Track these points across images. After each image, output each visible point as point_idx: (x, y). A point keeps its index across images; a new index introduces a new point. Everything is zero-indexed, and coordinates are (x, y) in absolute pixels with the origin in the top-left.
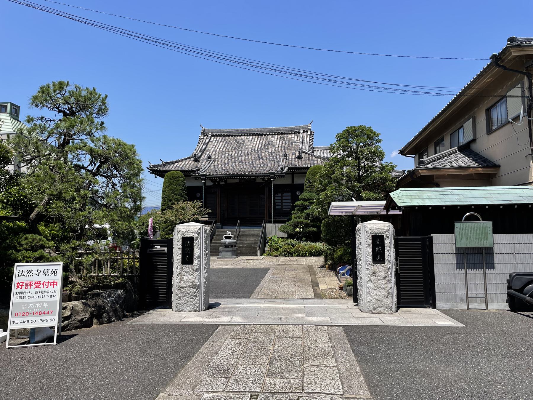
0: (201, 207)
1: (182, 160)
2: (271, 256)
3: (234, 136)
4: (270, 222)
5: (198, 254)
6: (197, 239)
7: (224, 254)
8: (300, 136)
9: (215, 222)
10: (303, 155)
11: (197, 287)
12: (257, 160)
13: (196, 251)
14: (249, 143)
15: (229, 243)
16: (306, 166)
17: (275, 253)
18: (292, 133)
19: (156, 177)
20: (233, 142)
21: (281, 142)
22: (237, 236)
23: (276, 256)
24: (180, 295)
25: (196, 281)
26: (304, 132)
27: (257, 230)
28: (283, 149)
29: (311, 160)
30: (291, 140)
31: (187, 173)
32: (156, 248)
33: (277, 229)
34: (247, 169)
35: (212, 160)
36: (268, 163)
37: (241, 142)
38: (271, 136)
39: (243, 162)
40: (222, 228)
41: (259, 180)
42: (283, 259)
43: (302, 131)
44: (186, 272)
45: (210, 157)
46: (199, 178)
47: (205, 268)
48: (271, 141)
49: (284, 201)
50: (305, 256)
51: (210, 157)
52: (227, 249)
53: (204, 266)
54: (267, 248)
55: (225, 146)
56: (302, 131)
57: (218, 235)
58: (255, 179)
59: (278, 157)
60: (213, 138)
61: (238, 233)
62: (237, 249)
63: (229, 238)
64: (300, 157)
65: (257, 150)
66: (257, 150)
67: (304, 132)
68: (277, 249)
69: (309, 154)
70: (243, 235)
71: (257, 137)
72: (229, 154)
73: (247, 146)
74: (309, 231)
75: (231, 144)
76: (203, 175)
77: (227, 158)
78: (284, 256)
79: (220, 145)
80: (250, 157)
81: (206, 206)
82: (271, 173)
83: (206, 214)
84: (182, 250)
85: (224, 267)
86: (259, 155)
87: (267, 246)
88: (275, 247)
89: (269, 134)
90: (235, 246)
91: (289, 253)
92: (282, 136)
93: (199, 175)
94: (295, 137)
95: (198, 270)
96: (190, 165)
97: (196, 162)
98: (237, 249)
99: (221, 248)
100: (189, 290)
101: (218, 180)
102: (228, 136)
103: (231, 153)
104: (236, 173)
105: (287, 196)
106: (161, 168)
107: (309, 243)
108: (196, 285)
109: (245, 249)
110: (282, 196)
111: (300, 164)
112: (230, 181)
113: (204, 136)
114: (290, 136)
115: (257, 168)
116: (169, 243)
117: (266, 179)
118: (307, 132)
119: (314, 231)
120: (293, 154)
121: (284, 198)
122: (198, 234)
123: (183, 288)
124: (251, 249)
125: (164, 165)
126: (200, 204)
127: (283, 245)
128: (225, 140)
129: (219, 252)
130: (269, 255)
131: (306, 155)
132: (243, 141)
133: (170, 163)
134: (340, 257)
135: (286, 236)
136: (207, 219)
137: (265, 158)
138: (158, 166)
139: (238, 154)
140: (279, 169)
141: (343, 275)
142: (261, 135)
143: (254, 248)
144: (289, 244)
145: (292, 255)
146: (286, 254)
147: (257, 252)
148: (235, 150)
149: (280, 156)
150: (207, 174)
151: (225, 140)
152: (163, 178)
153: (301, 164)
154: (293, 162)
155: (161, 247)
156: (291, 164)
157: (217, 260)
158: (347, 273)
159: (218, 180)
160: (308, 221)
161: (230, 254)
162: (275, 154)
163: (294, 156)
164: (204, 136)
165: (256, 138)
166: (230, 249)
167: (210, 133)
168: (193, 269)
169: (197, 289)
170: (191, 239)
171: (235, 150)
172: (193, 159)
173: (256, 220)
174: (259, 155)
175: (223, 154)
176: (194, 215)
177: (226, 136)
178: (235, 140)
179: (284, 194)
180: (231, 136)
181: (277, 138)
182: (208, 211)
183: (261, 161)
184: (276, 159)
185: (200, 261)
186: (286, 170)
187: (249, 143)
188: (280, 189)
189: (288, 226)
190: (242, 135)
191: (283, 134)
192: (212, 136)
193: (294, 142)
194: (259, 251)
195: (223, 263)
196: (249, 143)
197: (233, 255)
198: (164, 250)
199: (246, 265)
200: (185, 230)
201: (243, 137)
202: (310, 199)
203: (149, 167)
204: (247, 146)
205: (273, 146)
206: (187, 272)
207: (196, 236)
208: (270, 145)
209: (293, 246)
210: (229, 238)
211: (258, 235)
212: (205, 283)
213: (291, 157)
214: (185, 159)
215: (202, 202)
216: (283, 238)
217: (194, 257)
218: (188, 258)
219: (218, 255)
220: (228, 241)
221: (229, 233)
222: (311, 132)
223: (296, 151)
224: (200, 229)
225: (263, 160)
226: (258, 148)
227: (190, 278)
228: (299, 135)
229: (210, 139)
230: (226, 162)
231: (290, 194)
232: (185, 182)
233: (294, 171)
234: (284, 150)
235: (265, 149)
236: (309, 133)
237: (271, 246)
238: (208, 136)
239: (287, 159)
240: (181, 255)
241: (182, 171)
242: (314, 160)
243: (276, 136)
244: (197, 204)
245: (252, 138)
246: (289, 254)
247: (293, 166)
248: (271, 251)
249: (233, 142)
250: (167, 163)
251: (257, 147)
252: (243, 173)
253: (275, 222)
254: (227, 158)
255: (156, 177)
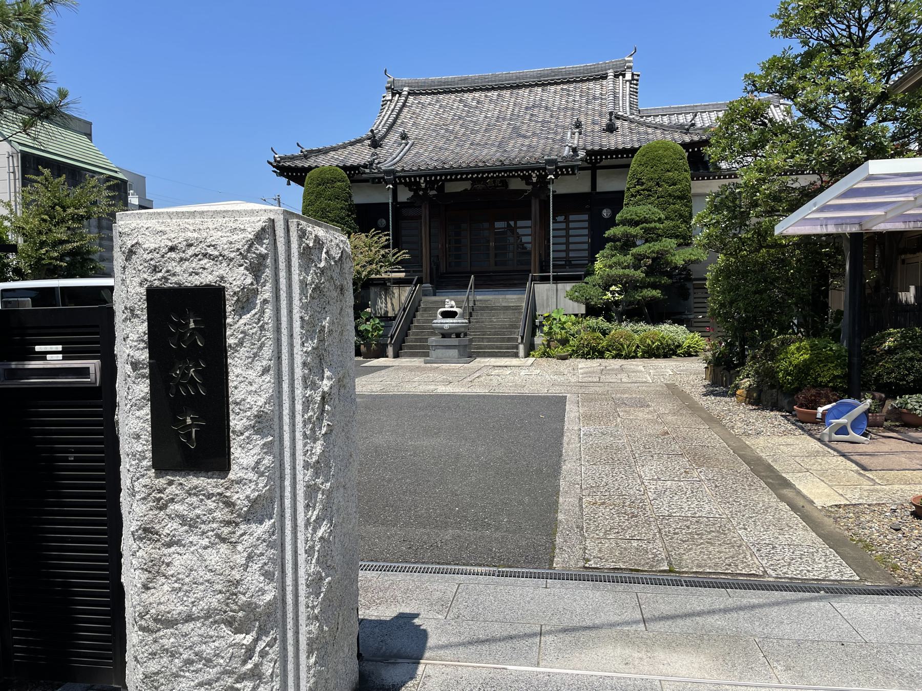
0: (387, 247)
1: (344, 146)
2: (549, 356)
3: (457, 91)
4: (545, 279)
5: (258, 402)
6: (246, 301)
7: (440, 352)
8: (609, 83)
9: (420, 281)
10: (618, 123)
11: (265, 620)
12: (510, 138)
13: (248, 384)
14: (492, 106)
15: (450, 328)
16: (629, 146)
17: (560, 350)
18: (588, 80)
19: (289, 184)
20: (456, 104)
21: (564, 99)
22: (470, 313)
23: (564, 358)
24: (153, 666)
25: (253, 579)
26: (616, 76)
27: (513, 298)
28: (569, 113)
29: (639, 133)
30: (588, 93)
31: (353, 172)
32: (42, 356)
33: (562, 295)
34: (488, 157)
35: (410, 142)
36: (538, 142)
37: (474, 104)
38: (540, 89)
39: (478, 144)
40: (435, 295)
41: (516, 184)
42: (583, 365)
43: (611, 74)
44: (184, 520)
45: (404, 137)
46: (379, 178)
47: (311, 490)
48: (542, 100)
49: (571, 232)
50: (633, 357)
51: (404, 137)
52: (447, 341)
53: (304, 477)
54: (540, 339)
55: (437, 114)
56: (611, 74)
57: (425, 310)
58: (504, 182)
59: (559, 130)
60: (411, 98)
61: (471, 304)
62: (471, 341)
63: (452, 315)
64: (611, 128)
65: (511, 119)
66: (511, 119)
67: (616, 76)
68: (564, 342)
69: (631, 122)
70: (483, 309)
71: (509, 92)
72: (447, 130)
73: (488, 111)
74: (644, 298)
75: (452, 109)
76: (388, 172)
77: (443, 137)
78: (584, 356)
79: (425, 114)
80: (494, 133)
81: (397, 244)
82: (549, 162)
83: (398, 263)
84: (152, 377)
85: (442, 389)
86: (516, 129)
87: (538, 333)
88: (559, 337)
89: (537, 85)
90: (465, 335)
91: (594, 349)
92: (565, 87)
93: (380, 172)
94: (595, 88)
95: (257, 510)
96: (360, 155)
97: (375, 147)
98: (471, 341)
99: (433, 340)
100: (206, 639)
101: (423, 185)
102: (445, 92)
103: (451, 127)
104: (464, 165)
105: (580, 223)
106: (299, 163)
107: (642, 326)
108: (249, 607)
109: (489, 340)
110: (567, 221)
111: (613, 142)
112: (452, 188)
113: (393, 95)
114: (585, 86)
115: (513, 155)
116: (88, 323)
117: (534, 180)
118: (624, 76)
119: (654, 299)
120: (594, 123)
121: (572, 225)
122: (256, 269)
123: (170, 623)
124: (503, 340)
125: (306, 156)
126: (384, 238)
127: (578, 332)
128: (437, 101)
129: (428, 347)
130: (545, 355)
131: (626, 123)
132: (478, 102)
133: (319, 152)
134: (803, 370)
135: (582, 309)
136: (402, 275)
137: (529, 134)
138: (293, 158)
139: (467, 129)
140: (566, 152)
141: (842, 430)
142: (518, 87)
143: (509, 340)
144: (594, 330)
145: (601, 355)
146: (588, 353)
147: (517, 347)
148: (461, 122)
149: (564, 127)
150: (399, 169)
151: (437, 101)
152: (303, 186)
153: (616, 143)
154: (597, 140)
155: (67, 354)
156: (592, 143)
157: (424, 369)
158: (855, 425)
159: (423, 185)
160: (639, 274)
161: (454, 353)
162: (553, 126)
163: (597, 128)
164: (393, 95)
165: (506, 93)
166: (454, 341)
167: (406, 89)
168: (229, 504)
169: (262, 632)
170: (208, 303)
171: (461, 122)
172: (368, 142)
173: (512, 277)
174: (516, 129)
175: (434, 131)
176: (370, 263)
177: (439, 93)
178: (461, 101)
179: (572, 217)
180: (452, 92)
181: (555, 92)
182: (403, 255)
183: (520, 141)
184: (556, 133)
185: (274, 448)
186: (582, 154)
187: (489, 105)
188: (569, 204)
189: (590, 288)
190: (475, 90)
191: (569, 82)
192: (409, 94)
193: (595, 98)
194: (521, 347)
195: (440, 377)
196: (492, 106)
197: (461, 355)
198: (84, 372)
199: (495, 382)
200: (164, 243)
201: (477, 94)
202: (646, 221)
203: (272, 161)
204: (488, 111)
205: (547, 108)
206: (191, 524)
207: (236, 278)
208: (540, 106)
209: (604, 333)
210: (452, 315)
211: (517, 308)
212: (315, 583)
213: (589, 129)
214: (352, 144)
215: (388, 235)
216: (576, 315)
217: (236, 422)
218: (195, 437)
219: (426, 355)
220: (448, 323)
221: (450, 304)
222: (633, 75)
223: (600, 115)
224: (267, 232)
225: (525, 137)
226: (512, 114)
227: (213, 557)
228: (604, 82)
229: (406, 101)
230: (441, 144)
231: (586, 217)
232: (352, 192)
233: (598, 161)
234: (572, 115)
235: (528, 117)
236: (628, 76)
237: (549, 334)
238: (400, 94)
239: (580, 133)
240: (147, 410)
241: (345, 168)
242: (648, 134)
243: (553, 88)
244: (375, 238)
245: (499, 95)
246: (595, 352)
247: (597, 148)
248: (549, 346)
249: (456, 104)
250: (311, 152)
251: (509, 112)
252: (480, 164)
253: (557, 279)
254: (443, 137)
255: (289, 184)
